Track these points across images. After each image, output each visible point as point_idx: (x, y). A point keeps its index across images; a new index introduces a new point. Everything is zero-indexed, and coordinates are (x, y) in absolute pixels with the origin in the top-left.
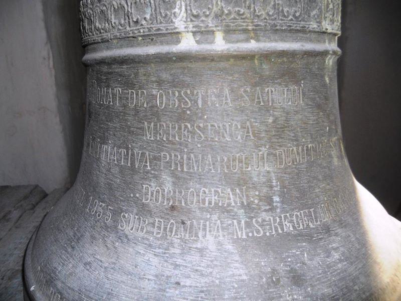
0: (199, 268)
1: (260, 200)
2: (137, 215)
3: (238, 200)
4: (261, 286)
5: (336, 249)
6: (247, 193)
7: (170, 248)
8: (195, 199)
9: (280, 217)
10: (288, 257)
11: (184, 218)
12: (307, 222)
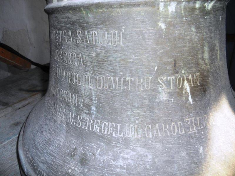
1: (84, 106)
4: (65, 153)
5: (124, 159)
6: (78, 99)
9: (94, 121)
12: (112, 132)
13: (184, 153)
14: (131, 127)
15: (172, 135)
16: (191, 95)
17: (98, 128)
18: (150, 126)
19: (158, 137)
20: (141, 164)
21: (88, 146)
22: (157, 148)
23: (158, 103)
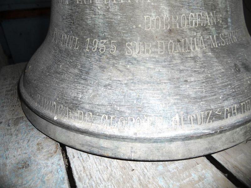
0: (195, 69)
2: (141, 42)
3: (212, 21)
6: (216, 15)
7: (173, 60)
8: (186, 22)
10: (239, 57)
11: (179, 38)
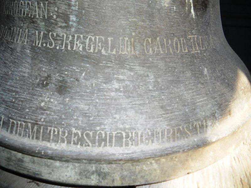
3: (41, 13)
4: (33, 84)
6: (49, 8)
12: (100, 48)
13: (189, 74)
14: (126, 40)
15: (174, 52)
16: (193, 6)
17: (80, 46)
18: (150, 40)
19: (159, 54)
20: (141, 86)
21: (67, 70)
22: (159, 67)
23: (159, 10)
